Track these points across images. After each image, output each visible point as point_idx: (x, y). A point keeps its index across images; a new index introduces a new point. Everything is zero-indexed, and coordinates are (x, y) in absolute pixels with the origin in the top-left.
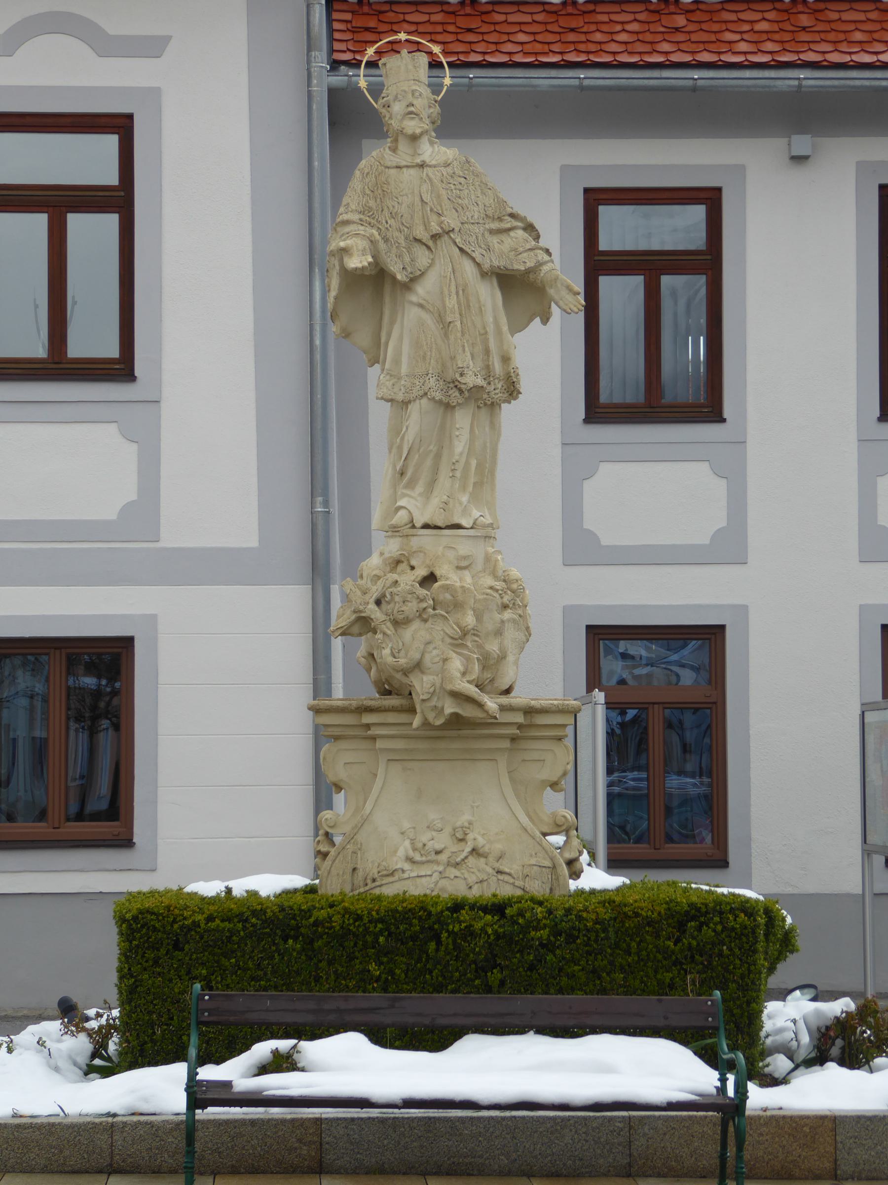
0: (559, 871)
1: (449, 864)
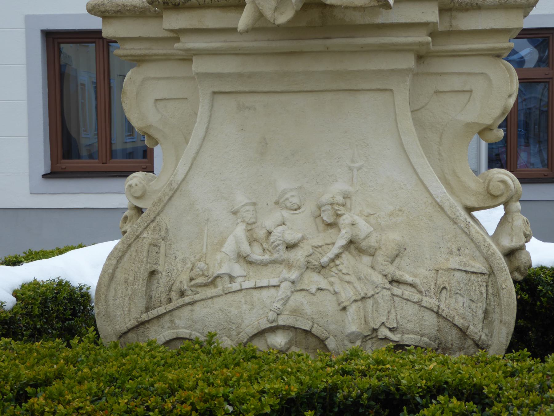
0: (500, 281)
1: (308, 266)
